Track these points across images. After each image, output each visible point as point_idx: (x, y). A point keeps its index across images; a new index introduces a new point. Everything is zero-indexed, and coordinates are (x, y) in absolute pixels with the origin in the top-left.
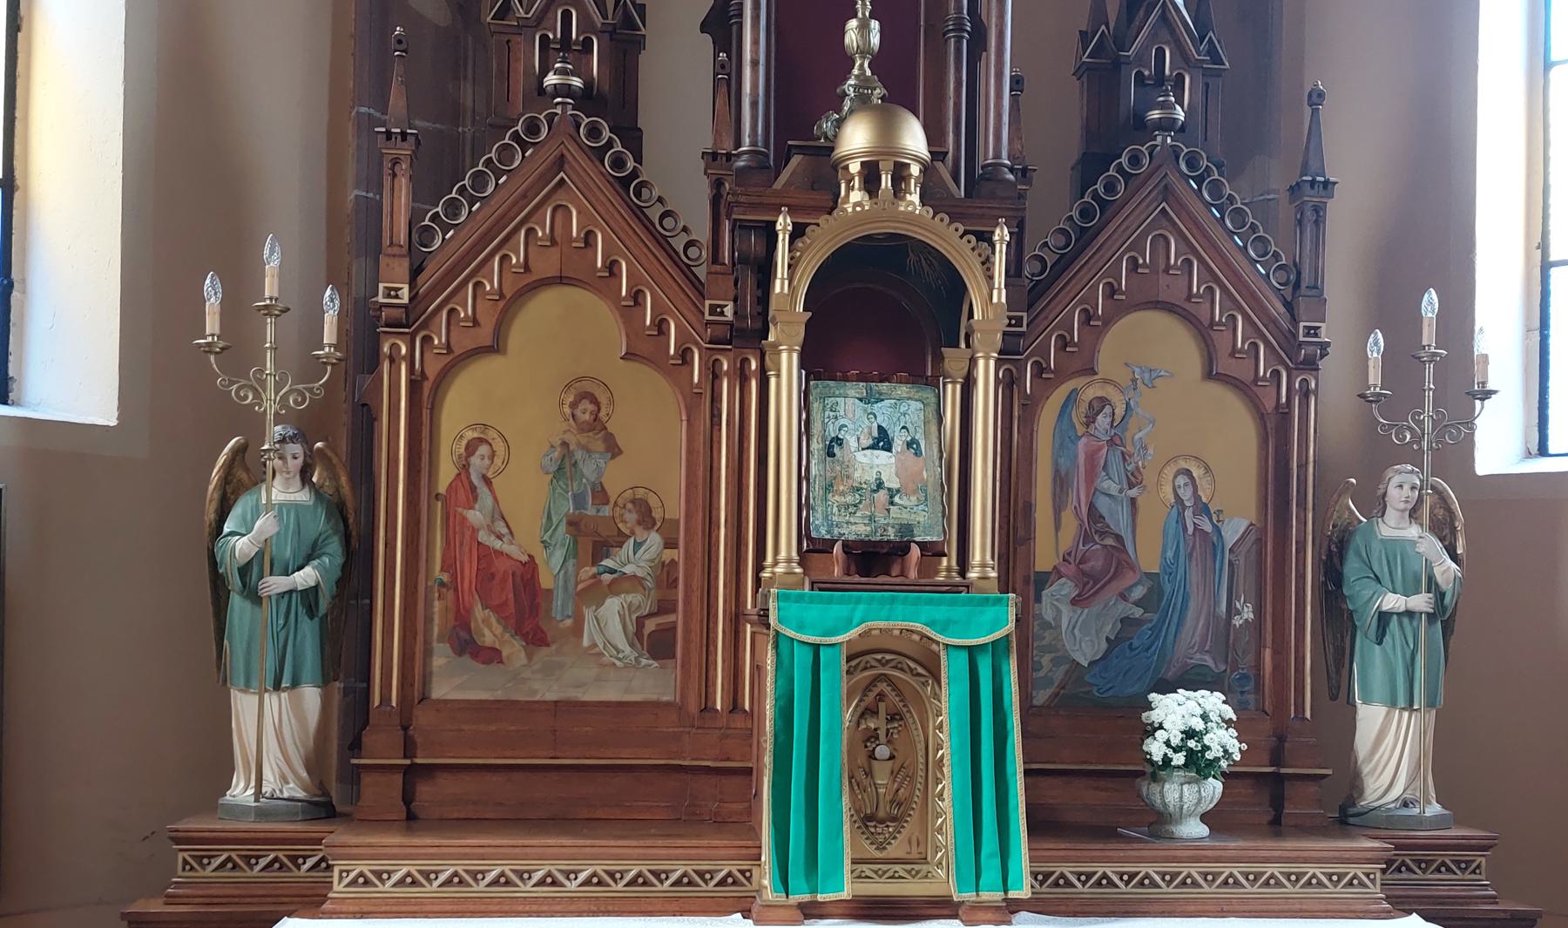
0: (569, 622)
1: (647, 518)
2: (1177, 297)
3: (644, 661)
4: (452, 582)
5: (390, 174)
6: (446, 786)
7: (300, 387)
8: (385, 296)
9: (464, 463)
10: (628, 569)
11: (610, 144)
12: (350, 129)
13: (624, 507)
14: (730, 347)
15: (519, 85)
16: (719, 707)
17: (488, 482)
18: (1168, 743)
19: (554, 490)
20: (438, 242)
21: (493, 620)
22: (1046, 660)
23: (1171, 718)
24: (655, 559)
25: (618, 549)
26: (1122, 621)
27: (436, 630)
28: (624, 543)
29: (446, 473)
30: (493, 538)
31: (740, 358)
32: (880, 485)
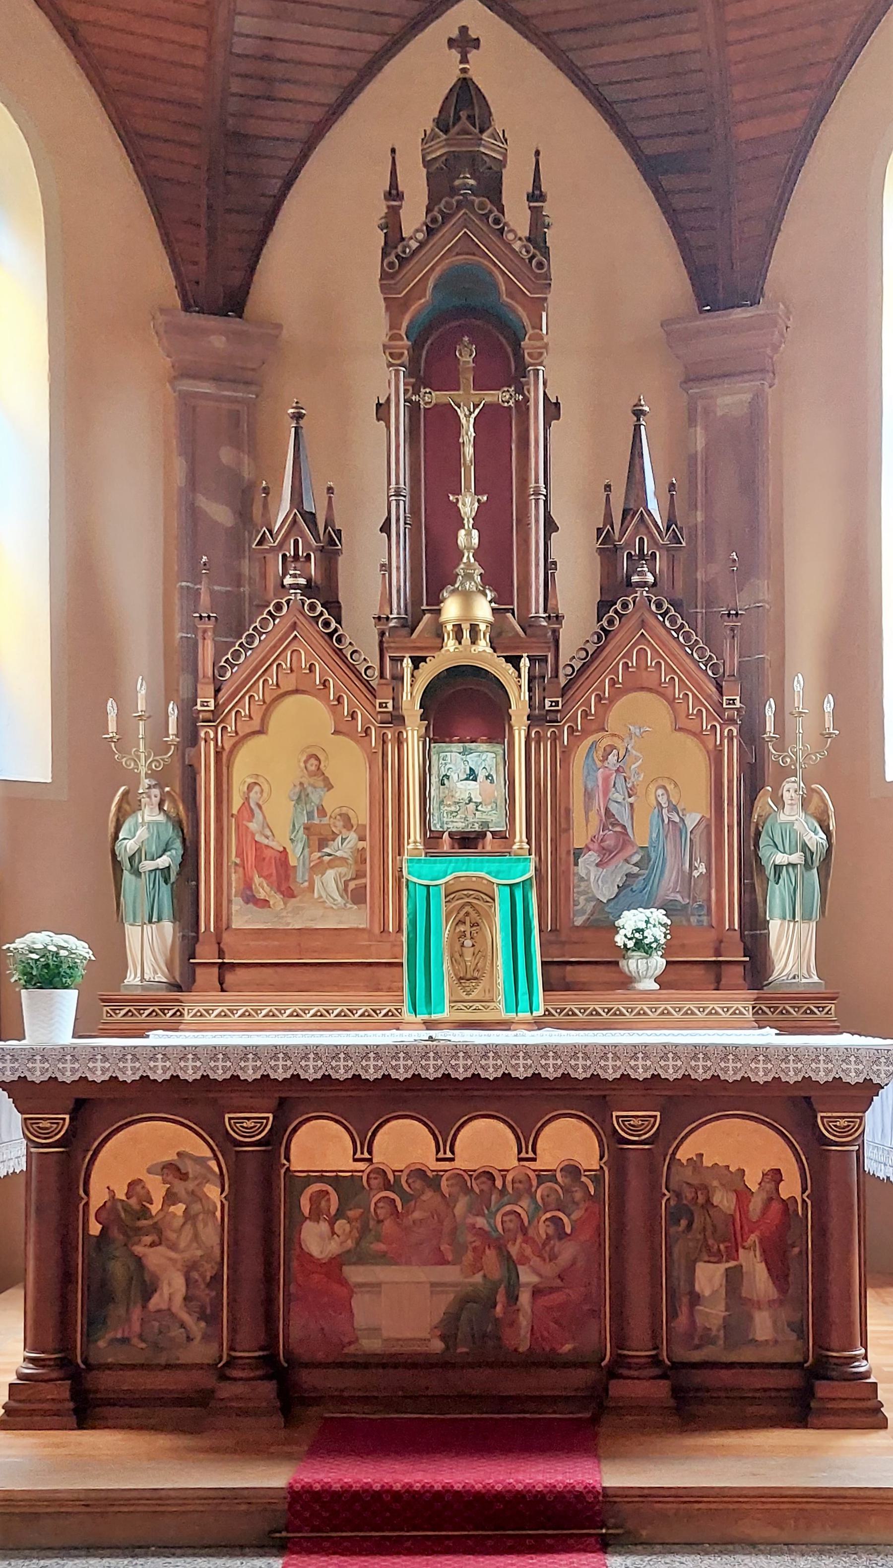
0: (306, 884)
1: (348, 823)
2: (653, 684)
3: (349, 906)
6: (241, 973)
7: (158, 758)
10: (338, 854)
11: (322, 614)
12: (177, 596)
15: (271, 583)
16: (391, 930)
17: (260, 807)
18: (625, 936)
20: (228, 674)
22: (582, 899)
23: (629, 922)
26: (626, 875)
29: (237, 803)
32: (470, 801)
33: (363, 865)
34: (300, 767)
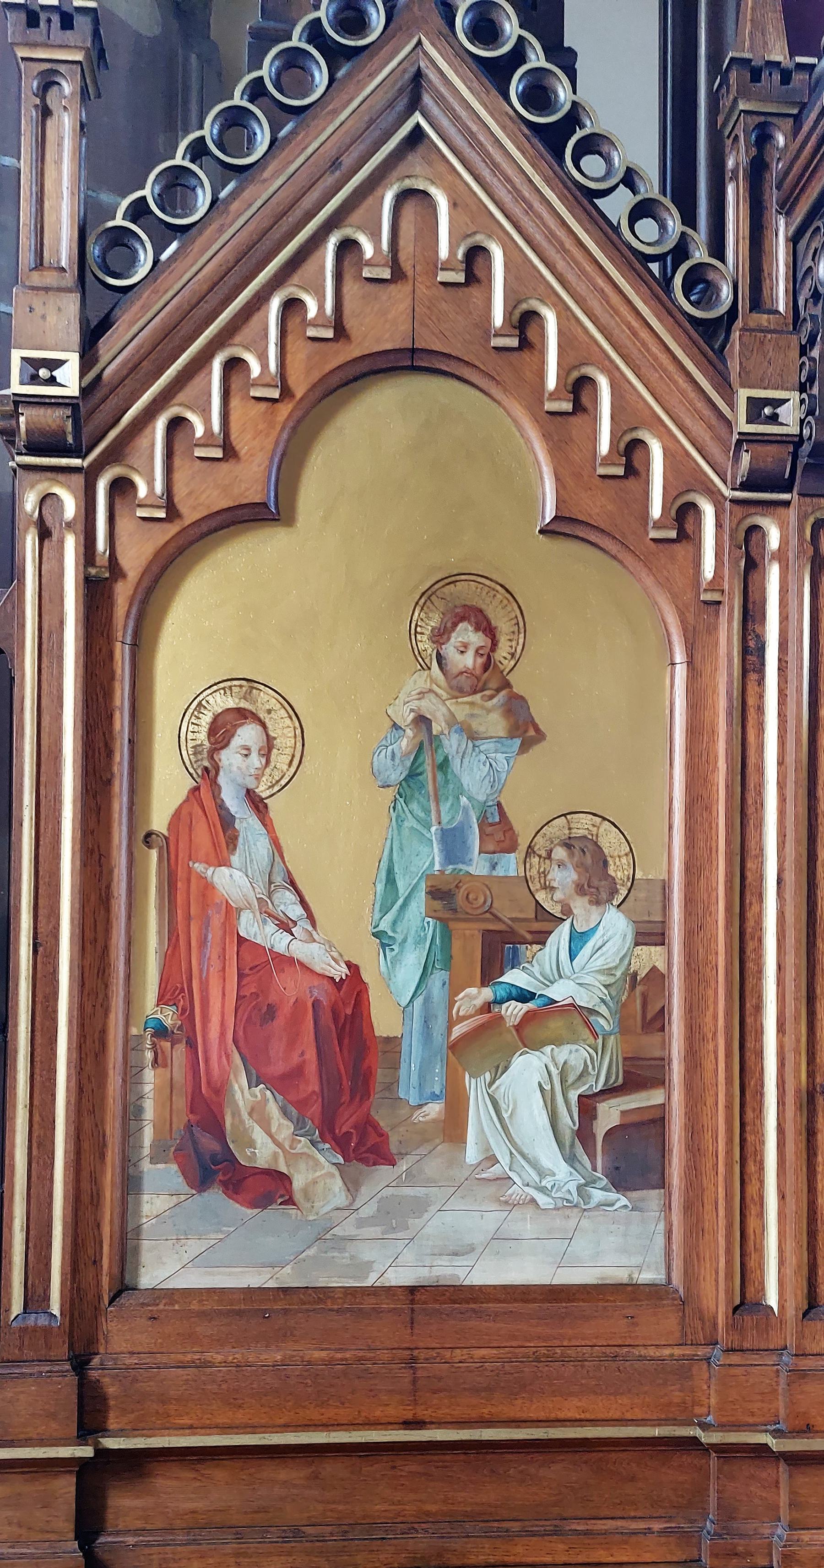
0: (435, 1110)
3: (597, 1195)
4: (180, 1028)
5: (36, 106)
8: (26, 378)
9: (206, 763)
10: (560, 992)
11: (518, 55)
13: (549, 856)
14: (786, 496)
16: (772, 1299)
19: (400, 821)
21: (273, 1109)
24: (616, 968)
25: (536, 947)
27: (148, 1135)
28: (550, 933)
30: (271, 927)
31: (812, 520)
33: (656, 1038)
34: (418, 655)
